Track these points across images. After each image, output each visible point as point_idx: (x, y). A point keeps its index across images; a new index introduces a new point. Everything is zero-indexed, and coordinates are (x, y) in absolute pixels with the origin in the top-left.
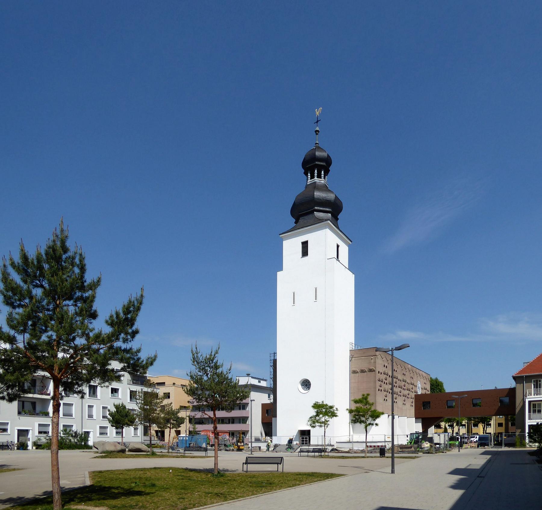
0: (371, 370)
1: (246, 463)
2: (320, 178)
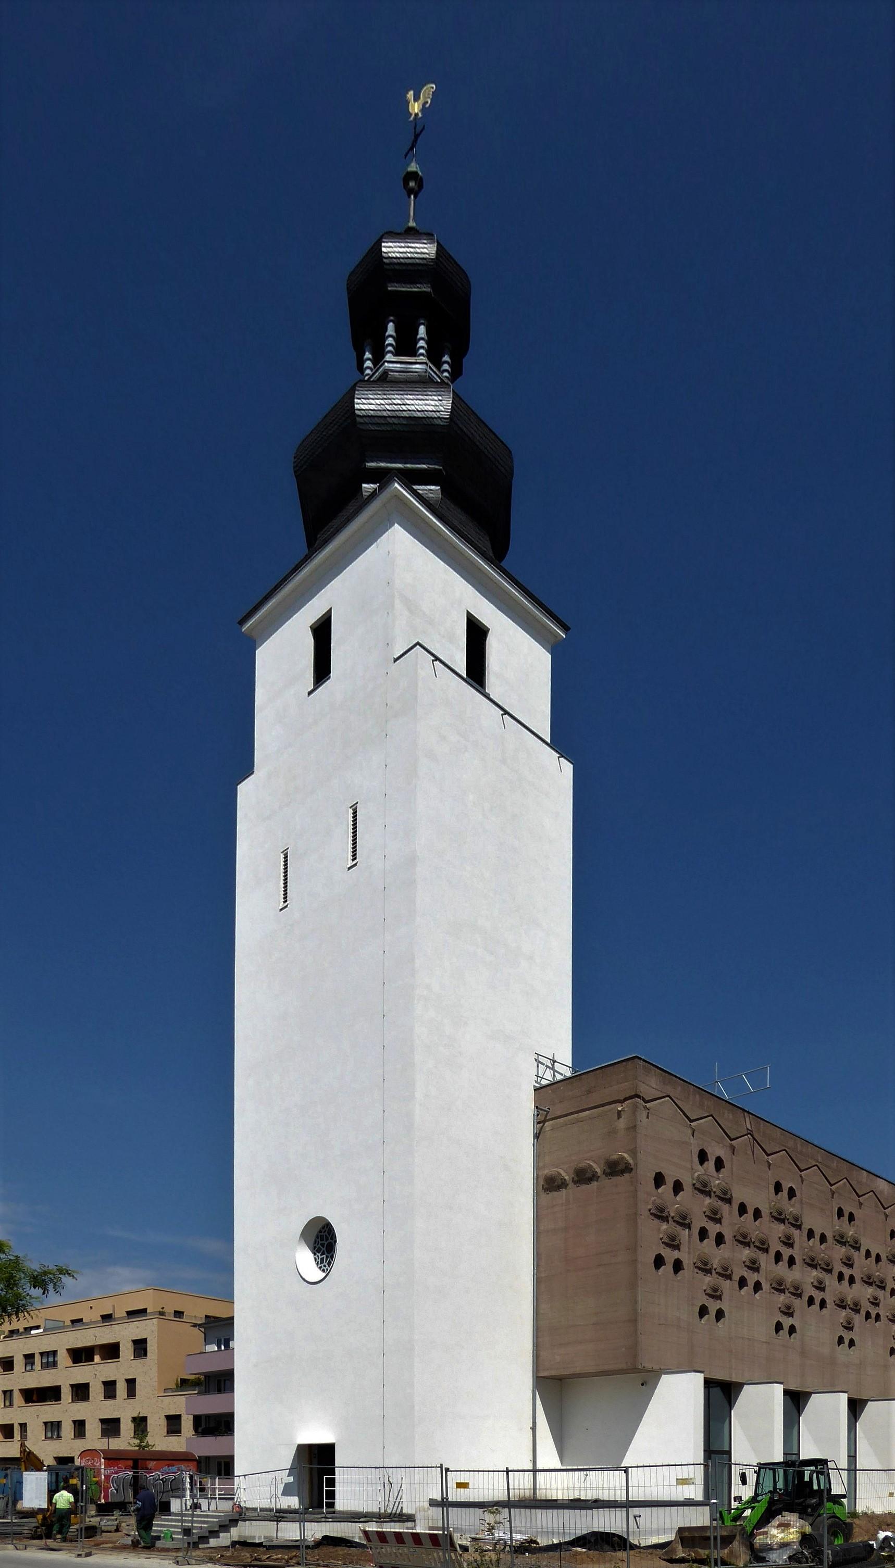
0: (616, 1168)
2: (413, 352)
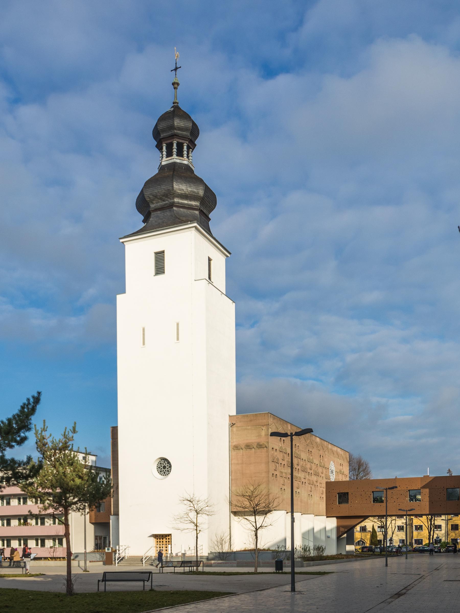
1: (103, 581)
